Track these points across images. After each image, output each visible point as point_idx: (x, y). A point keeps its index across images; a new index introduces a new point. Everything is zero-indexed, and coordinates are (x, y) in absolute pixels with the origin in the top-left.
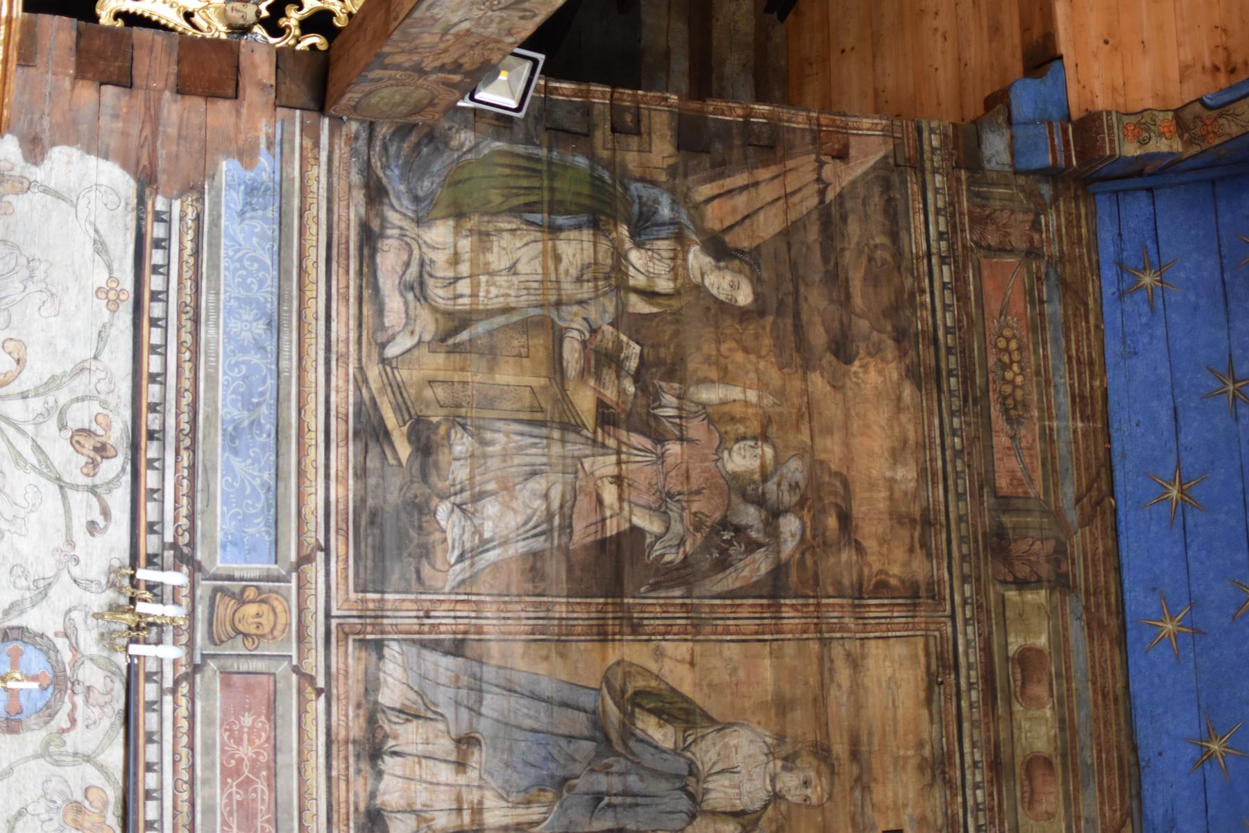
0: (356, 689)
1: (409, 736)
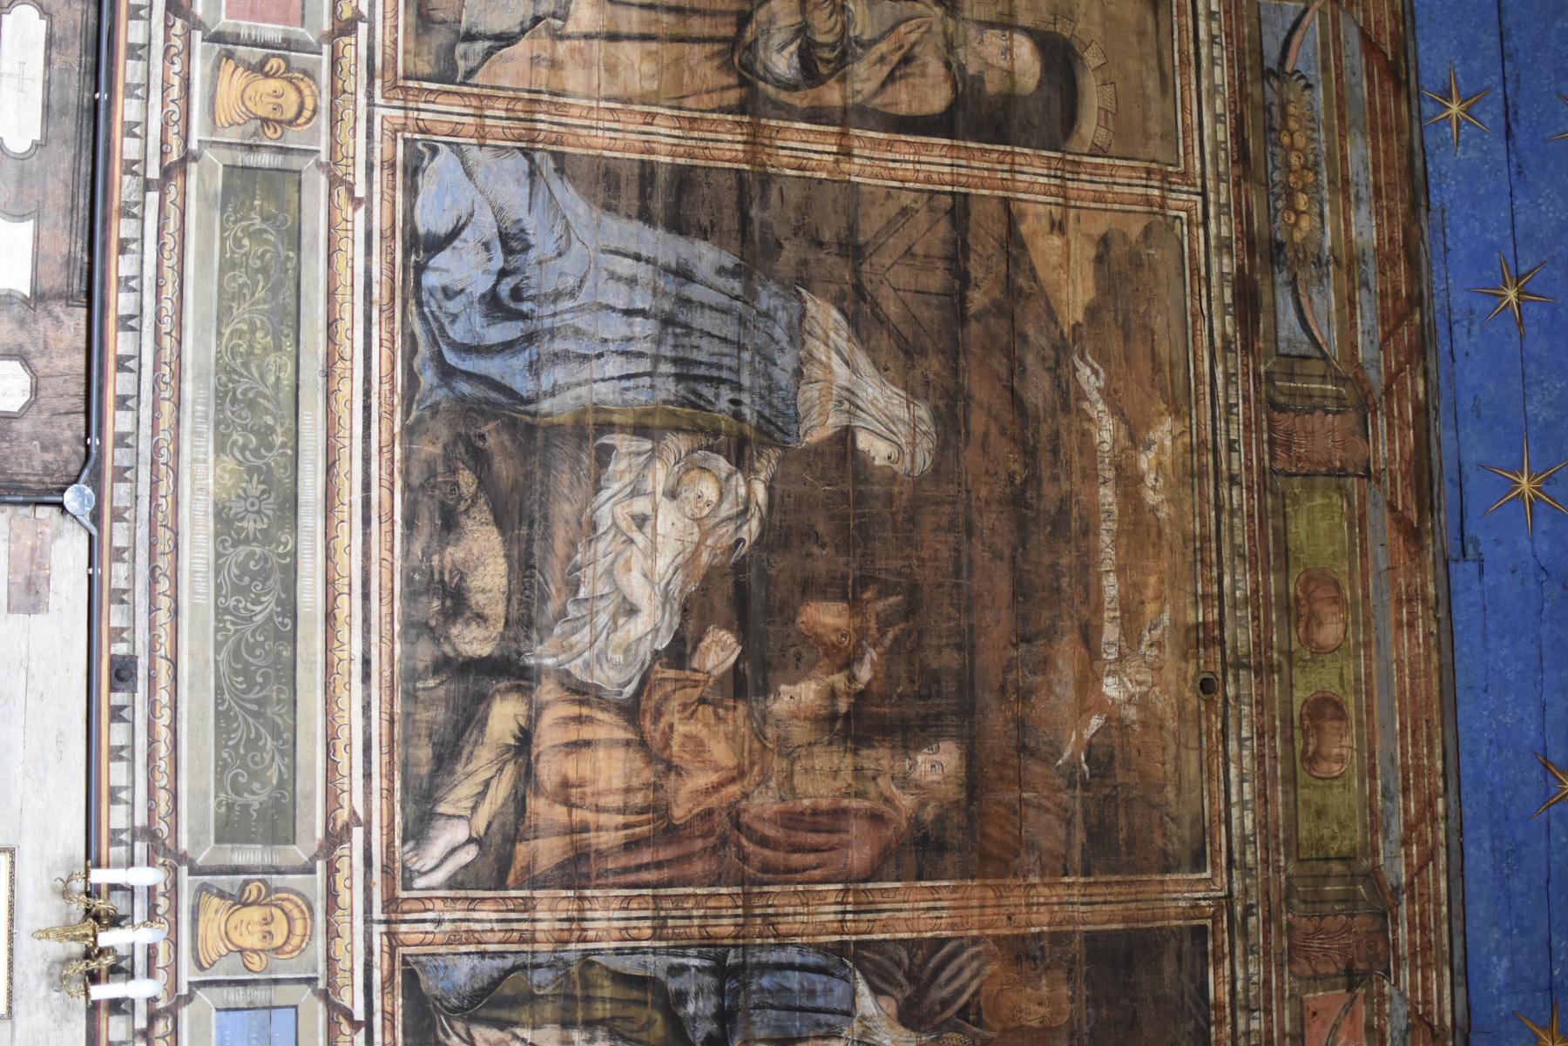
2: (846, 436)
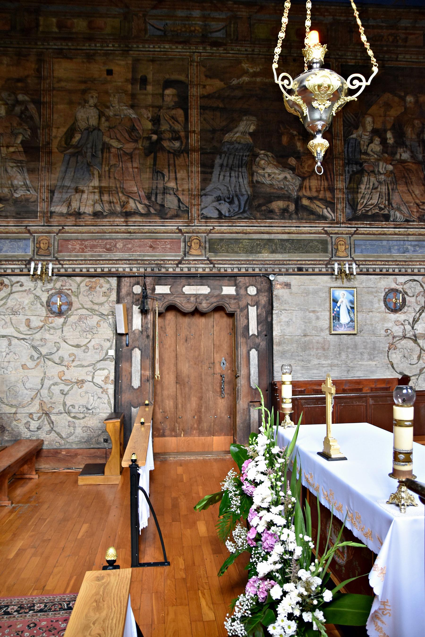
0: (62, 219)
1: (75, 205)
2: (250, 134)
